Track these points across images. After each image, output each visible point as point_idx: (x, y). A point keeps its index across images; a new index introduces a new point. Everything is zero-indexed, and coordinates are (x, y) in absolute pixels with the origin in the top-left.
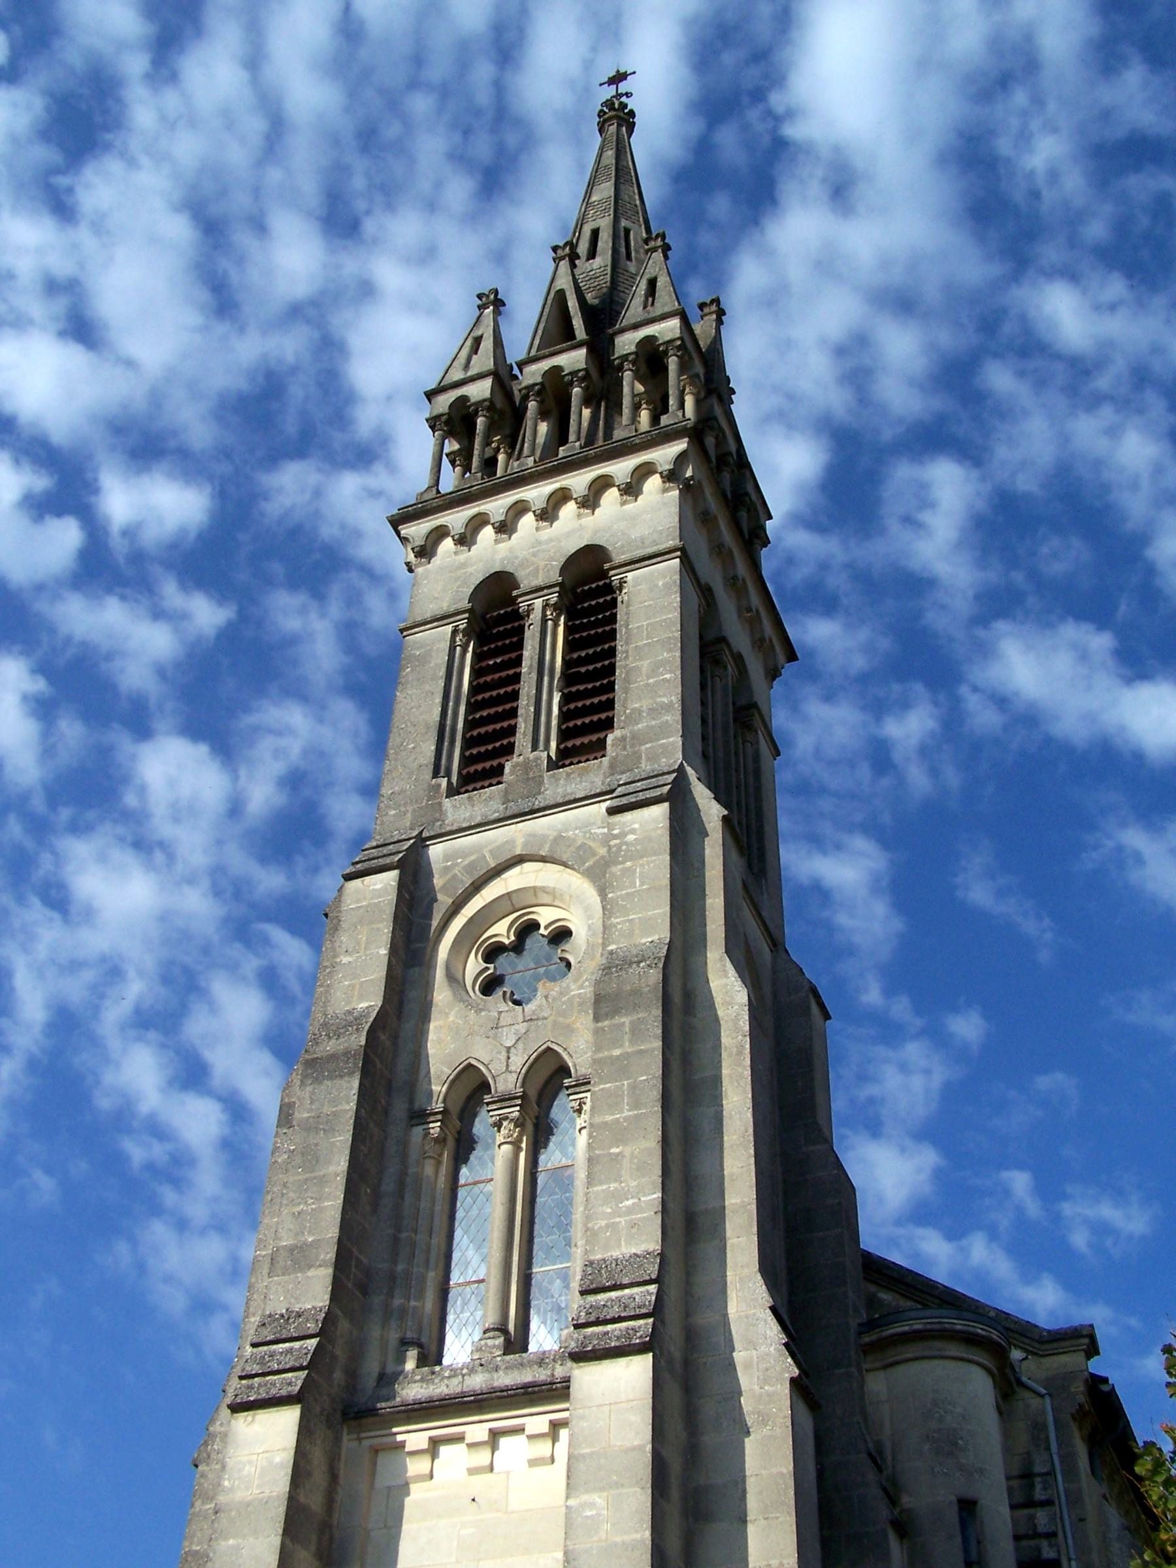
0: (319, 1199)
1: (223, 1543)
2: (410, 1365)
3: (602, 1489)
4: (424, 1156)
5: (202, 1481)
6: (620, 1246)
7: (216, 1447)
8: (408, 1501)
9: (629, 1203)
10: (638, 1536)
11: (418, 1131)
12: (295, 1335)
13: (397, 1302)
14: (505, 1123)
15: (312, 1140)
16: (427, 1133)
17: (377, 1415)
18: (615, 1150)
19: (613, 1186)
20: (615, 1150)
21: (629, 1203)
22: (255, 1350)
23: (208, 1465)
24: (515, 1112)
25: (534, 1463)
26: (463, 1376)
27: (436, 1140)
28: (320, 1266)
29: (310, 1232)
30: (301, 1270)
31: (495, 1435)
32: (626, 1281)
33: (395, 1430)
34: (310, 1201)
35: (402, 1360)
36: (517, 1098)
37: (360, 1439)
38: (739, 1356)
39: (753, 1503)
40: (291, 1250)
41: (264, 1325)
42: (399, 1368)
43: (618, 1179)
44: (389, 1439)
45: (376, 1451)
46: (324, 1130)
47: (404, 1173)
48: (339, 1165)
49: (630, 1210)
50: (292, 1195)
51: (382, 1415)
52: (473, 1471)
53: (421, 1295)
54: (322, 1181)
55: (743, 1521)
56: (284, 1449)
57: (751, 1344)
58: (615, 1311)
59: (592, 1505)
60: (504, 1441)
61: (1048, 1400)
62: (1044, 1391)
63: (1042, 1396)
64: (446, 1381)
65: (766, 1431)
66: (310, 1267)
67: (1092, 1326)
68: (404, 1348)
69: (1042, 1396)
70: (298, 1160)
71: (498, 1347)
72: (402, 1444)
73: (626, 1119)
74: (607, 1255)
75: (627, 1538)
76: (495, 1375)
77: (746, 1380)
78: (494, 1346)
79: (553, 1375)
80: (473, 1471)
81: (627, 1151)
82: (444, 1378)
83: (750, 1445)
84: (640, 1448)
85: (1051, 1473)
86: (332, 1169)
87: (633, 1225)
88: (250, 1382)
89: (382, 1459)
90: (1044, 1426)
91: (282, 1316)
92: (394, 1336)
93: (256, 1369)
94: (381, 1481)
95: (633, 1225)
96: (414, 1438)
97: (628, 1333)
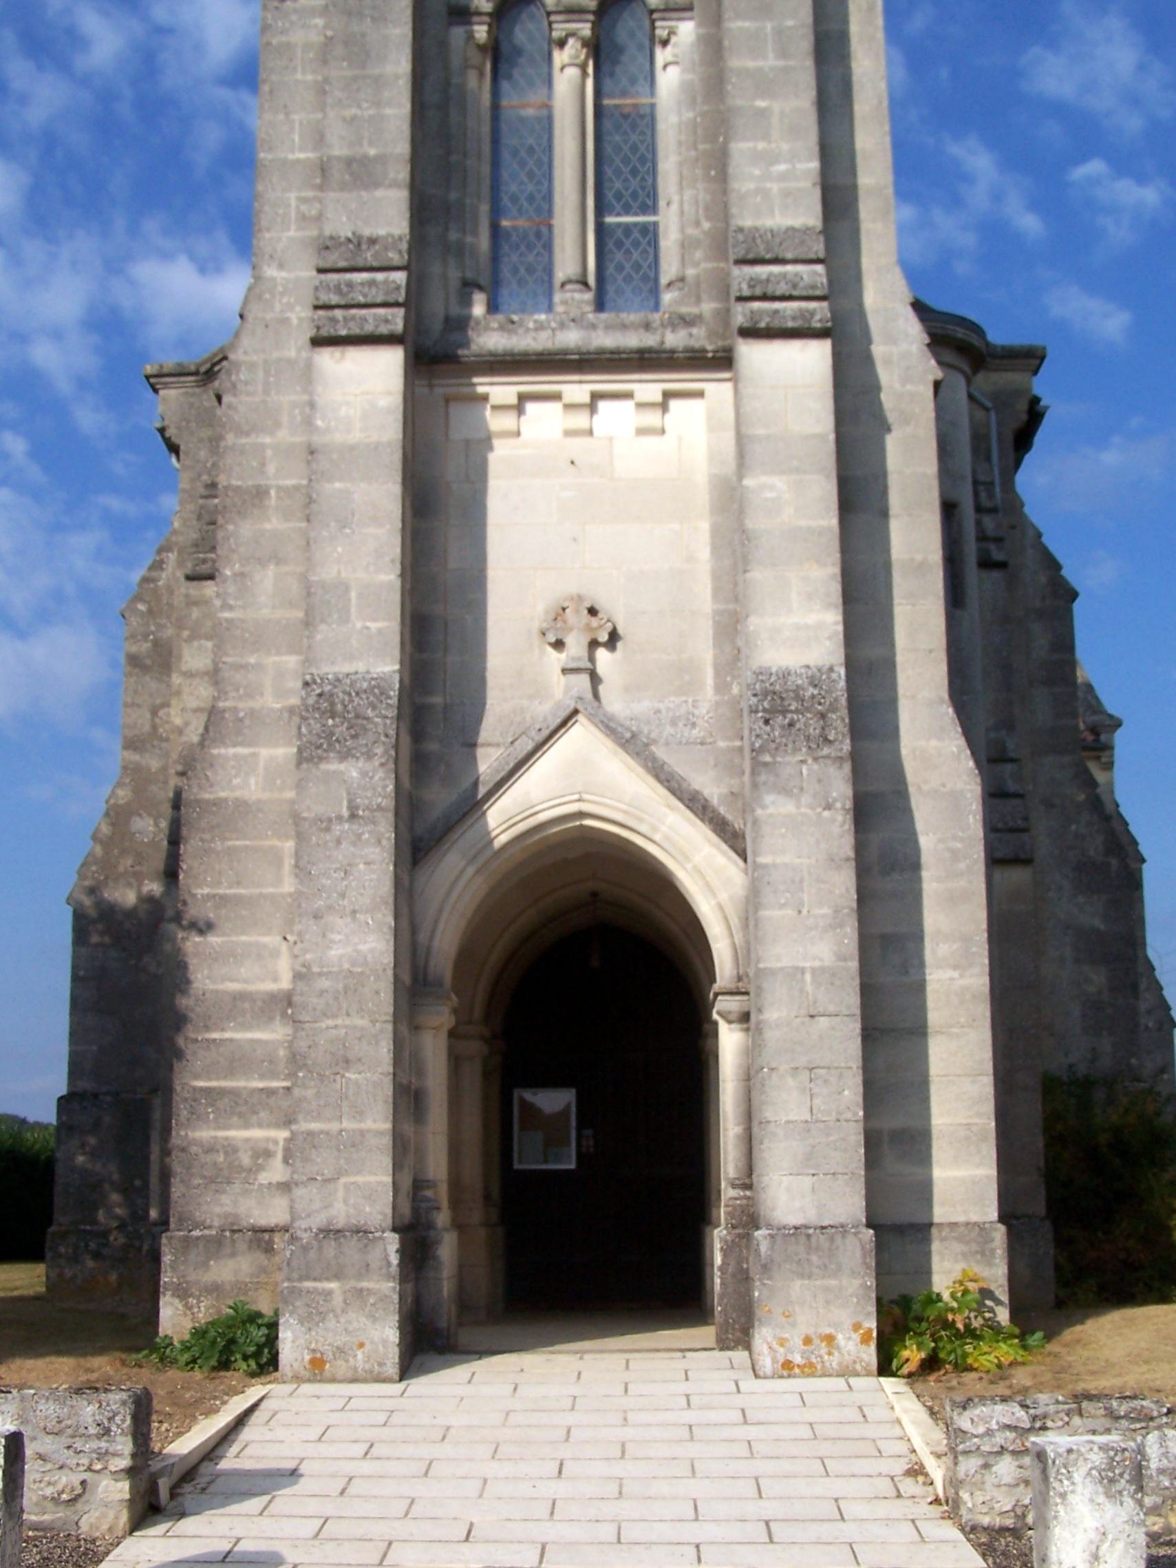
0: (377, 104)
1: (327, 486)
2: (478, 310)
3: (783, 472)
4: (466, 66)
5: (231, 413)
6: (772, 212)
7: (242, 377)
8: (492, 458)
9: (782, 167)
10: (824, 523)
11: (457, 33)
12: (375, 264)
13: (453, 236)
14: (571, 41)
15: (355, 28)
16: (470, 36)
17: (460, 363)
18: (761, 104)
19: (761, 145)
20: (761, 104)
21: (782, 167)
22: (323, 276)
23: (235, 395)
24: (586, 29)
25: (642, 432)
26: (553, 330)
27: (482, 48)
28: (390, 186)
29: (371, 144)
30: (366, 187)
31: (596, 397)
32: (789, 256)
33: (476, 380)
34: (365, 105)
35: (467, 302)
36: (588, 12)
37: (431, 386)
38: (878, 350)
39: (895, 500)
40: (349, 162)
41: (327, 248)
42: (465, 312)
43: (766, 137)
44: (465, 390)
45: (447, 400)
46: (373, 18)
47: (448, 84)
48: (399, 65)
49: (783, 177)
50: (338, 94)
51: (466, 363)
52: (569, 433)
53: (475, 233)
54: (379, 82)
55: (884, 514)
56: (389, 393)
57: (891, 339)
58: (782, 289)
59: (772, 488)
60: (602, 405)
61: (993, 415)
62: (988, 404)
63: (987, 409)
64: (533, 334)
65: (909, 430)
66: (377, 185)
67: (1044, 348)
68: (467, 290)
69: (987, 409)
70: (339, 50)
71: (587, 303)
72: (485, 398)
73: (772, 69)
74: (759, 223)
75: (814, 524)
76: (593, 334)
77: (885, 376)
78: (582, 301)
79: (663, 343)
80: (569, 433)
81: (776, 107)
82: (528, 330)
83: (892, 443)
84: (822, 437)
85: (992, 483)
86: (389, 69)
87: (786, 194)
88: (330, 313)
89: (456, 410)
90: (987, 437)
91: (349, 240)
92: (454, 275)
93: (334, 299)
94: (458, 432)
95: (786, 194)
96: (500, 390)
97: (802, 314)
